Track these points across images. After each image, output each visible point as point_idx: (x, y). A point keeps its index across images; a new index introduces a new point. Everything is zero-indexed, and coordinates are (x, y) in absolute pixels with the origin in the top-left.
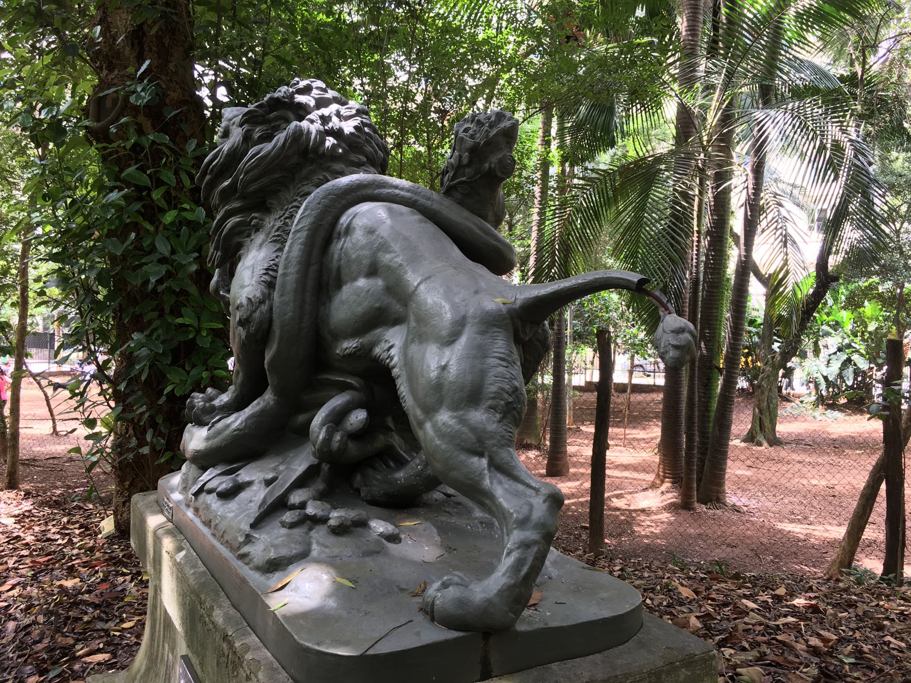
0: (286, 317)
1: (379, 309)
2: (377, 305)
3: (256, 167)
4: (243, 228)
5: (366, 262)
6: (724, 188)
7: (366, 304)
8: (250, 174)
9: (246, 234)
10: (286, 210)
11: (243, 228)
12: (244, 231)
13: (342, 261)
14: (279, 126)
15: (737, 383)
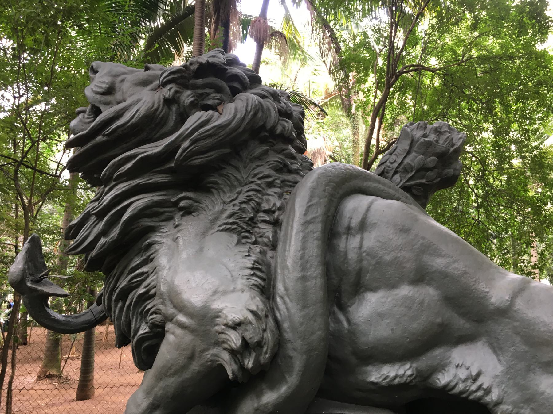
0: (314, 337)
1: (441, 325)
2: (439, 320)
3: (210, 136)
4: (162, 210)
5: (409, 266)
6: (101, 220)
7: (423, 318)
8: (201, 144)
9: (163, 217)
10: (239, 193)
11: (162, 210)
12: (163, 213)
13: (365, 263)
14: (208, 94)
15: (85, 336)
